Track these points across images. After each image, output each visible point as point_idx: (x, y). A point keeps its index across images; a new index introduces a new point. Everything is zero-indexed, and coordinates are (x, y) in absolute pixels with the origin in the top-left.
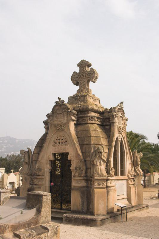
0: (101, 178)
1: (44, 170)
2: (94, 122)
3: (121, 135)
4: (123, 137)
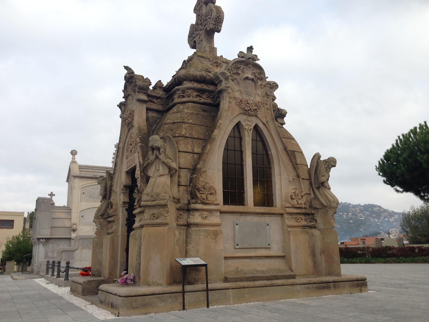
0: (154, 203)
1: (117, 205)
4: (264, 124)
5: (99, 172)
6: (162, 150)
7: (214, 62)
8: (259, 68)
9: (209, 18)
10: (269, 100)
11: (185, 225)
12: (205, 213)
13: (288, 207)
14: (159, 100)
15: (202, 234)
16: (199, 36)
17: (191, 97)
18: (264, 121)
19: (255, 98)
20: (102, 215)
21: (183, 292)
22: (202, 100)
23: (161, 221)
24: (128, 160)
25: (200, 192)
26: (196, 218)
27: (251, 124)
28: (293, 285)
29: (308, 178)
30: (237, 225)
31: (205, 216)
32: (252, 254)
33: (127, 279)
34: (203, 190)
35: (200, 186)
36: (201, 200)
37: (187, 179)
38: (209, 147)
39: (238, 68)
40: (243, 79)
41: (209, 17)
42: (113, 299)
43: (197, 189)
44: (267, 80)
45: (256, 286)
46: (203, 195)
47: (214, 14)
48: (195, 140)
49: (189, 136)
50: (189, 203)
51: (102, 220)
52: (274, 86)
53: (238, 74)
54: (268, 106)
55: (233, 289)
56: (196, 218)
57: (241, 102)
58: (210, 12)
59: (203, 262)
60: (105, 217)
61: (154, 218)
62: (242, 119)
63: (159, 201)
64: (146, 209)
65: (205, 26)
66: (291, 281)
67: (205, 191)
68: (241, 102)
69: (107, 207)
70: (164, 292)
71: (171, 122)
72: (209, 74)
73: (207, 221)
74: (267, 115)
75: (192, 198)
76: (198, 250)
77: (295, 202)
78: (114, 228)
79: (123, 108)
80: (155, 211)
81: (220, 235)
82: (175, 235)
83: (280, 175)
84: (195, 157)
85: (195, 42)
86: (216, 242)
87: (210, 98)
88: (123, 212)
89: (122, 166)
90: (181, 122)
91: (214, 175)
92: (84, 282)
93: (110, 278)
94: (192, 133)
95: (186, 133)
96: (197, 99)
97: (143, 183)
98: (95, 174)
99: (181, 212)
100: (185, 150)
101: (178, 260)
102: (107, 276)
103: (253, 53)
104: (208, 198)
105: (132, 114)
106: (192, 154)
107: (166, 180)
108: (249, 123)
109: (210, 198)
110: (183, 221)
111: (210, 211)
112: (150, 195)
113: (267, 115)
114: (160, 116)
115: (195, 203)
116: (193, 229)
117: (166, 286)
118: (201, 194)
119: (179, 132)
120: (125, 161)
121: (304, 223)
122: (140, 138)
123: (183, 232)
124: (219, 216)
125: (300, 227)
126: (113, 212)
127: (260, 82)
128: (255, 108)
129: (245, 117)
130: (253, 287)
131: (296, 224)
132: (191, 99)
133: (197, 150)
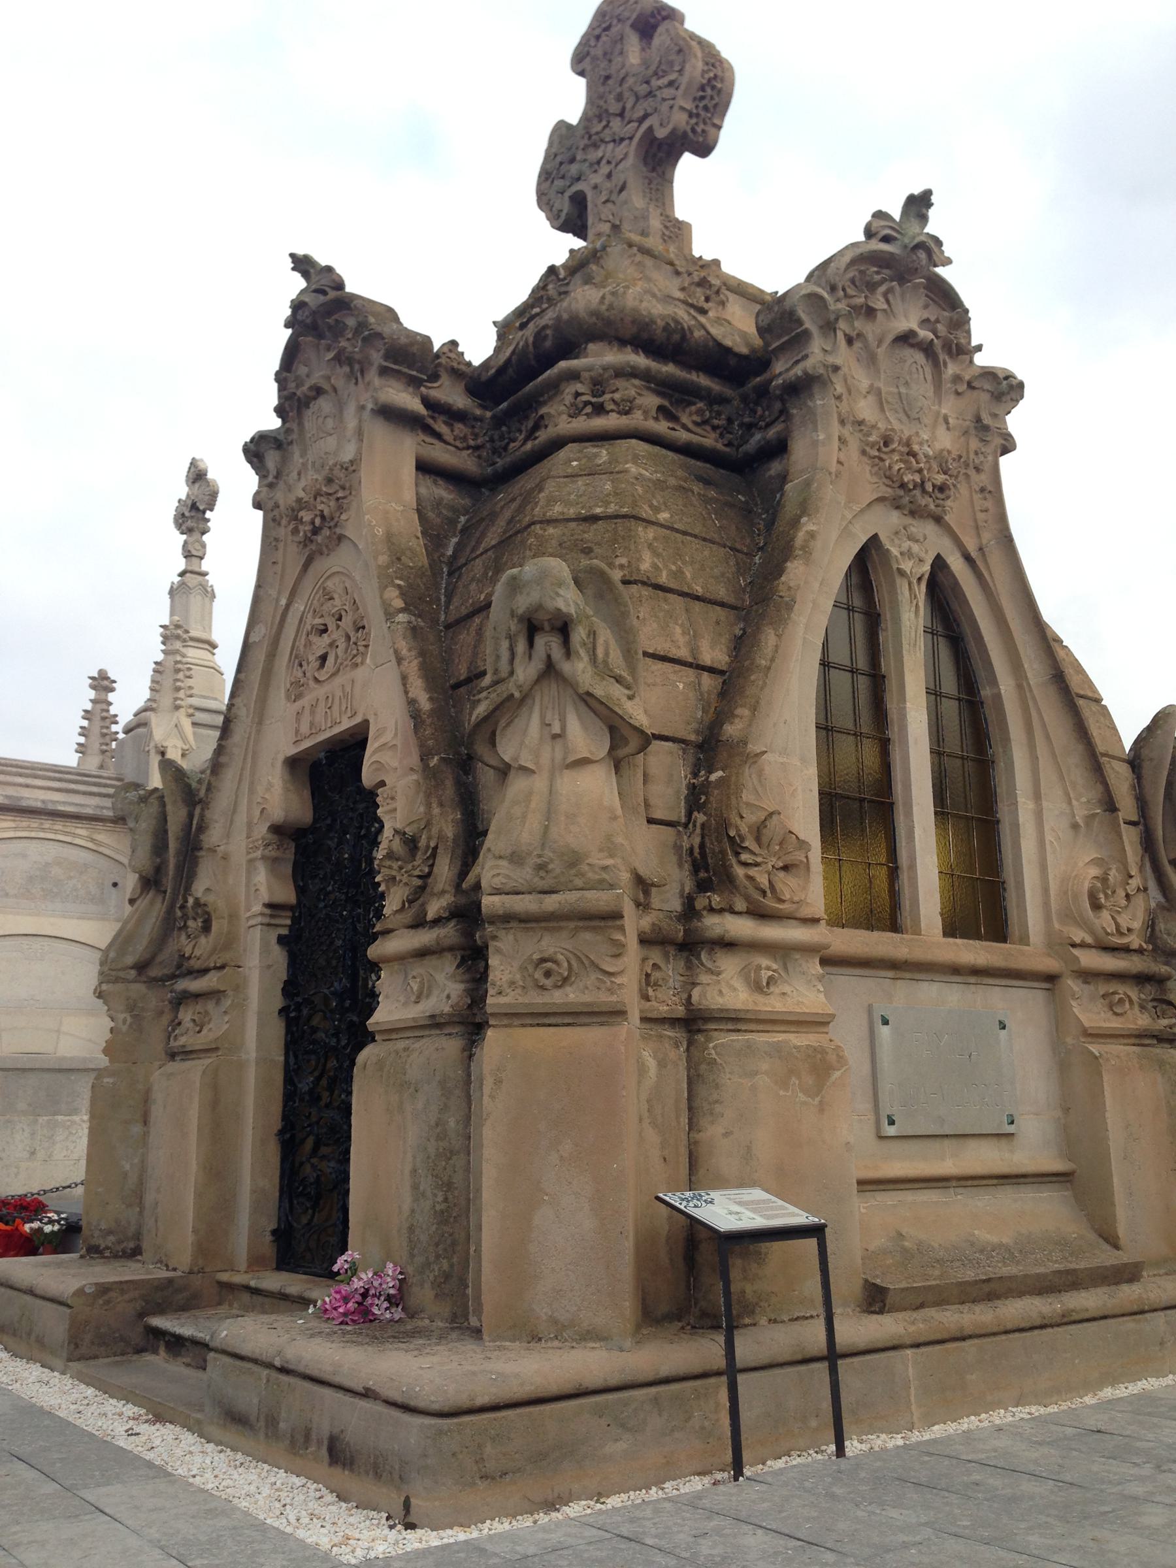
0: (551, 903)
1: (233, 917)
2: (611, 422)
3: (928, 529)
4: (968, 558)
5: (27, 786)
6: (579, 635)
7: (696, 279)
8: (946, 298)
9: (671, 84)
10: (989, 449)
11: (673, 1022)
12: (765, 962)
13: (1083, 945)
14: (460, 428)
15: (765, 1066)
16: (605, 169)
17: (638, 415)
18: (972, 548)
19: (934, 438)
20: (141, 967)
21: (731, 1371)
22: (683, 436)
23: (587, 998)
24: (305, 701)
25: (744, 857)
26: (726, 987)
27: (922, 555)
28: (1142, 1312)
29: (1135, 818)
30: (885, 1022)
31: (765, 975)
32: (948, 1166)
33: (365, 1295)
34: (753, 846)
35: (744, 829)
36: (747, 898)
37: (678, 792)
38: (769, 638)
39: (872, 287)
40: (890, 337)
41: (673, 77)
42: (355, 1420)
43: (731, 839)
44: (980, 360)
45: (1009, 1326)
46: (752, 872)
47: (696, 67)
48: (697, 606)
49: (672, 586)
50: (689, 912)
51: (139, 988)
52: (1005, 389)
53: (870, 312)
54: (983, 477)
55: (917, 1346)
56: (726, 987)
57: (886, 444)
58: (673, 57)
59: (800, 1218)
60: (154, 972)
61: (548, 983)
62: (885, 523)
63: (578, 894)
64: (501, 934)
65: (641, 120)
66: (1128, 1294)
67: (764, 852)
68: (886, 444)
69: (170, 925)
70: (627, 1378)
71: (572, 512)
72: (702, 319)
73: (773, 1004)
74: (981, 516)
75: (703, 886)
76: (749, 1148)
77: (1105, 920)
78: (217, 1027)
79: (272, 459)
80: (549, 944)
81: (837, 1074)
82: (642, 1070)
83: (1037, 796)
84: (705, 688)
85: (579, 201)
86: (821, 1109)
87: (714, 428)
88: (265, 949)
89: (258, 732)
90: (624, 516)
91: (786, 777)
92: (80, 1292)
93: (201, 1271)
94: (680, 571)
95: (655, 566)
96: (662, 427)
97: (441, 805)
98: (11, 791)
99: (656, 956)
100: (660, 645)
101: (674, 1199)
102: (183, 1256)
103: (930, 229)
104: (779, 886)
105: (340, 484)
106: (691, 671)
107: (596, 786)
108: (916, 548)
109: (788, 885)
110: (667, 1003)
111: (782, 951)
112: (532, 861)
113: (981, 516)
114: (466, 502)
115: (721, 911)
116: (721, 1040)
117: (628, 1343)
118: (745, 864)
119: (624, 561)
120: (280, 706)
121: (1142, 1021)
122: (399, 586)
123: (673, 1054)
124: (820, 978)
125: (1129, 1036)
126: (213, 951)
127: (951, 369)
128: (940, 478)
129: (895, 518)
130: (994, 1334)
131: (1115, 1024)
132: (637, 420)
133: (714, 653)
